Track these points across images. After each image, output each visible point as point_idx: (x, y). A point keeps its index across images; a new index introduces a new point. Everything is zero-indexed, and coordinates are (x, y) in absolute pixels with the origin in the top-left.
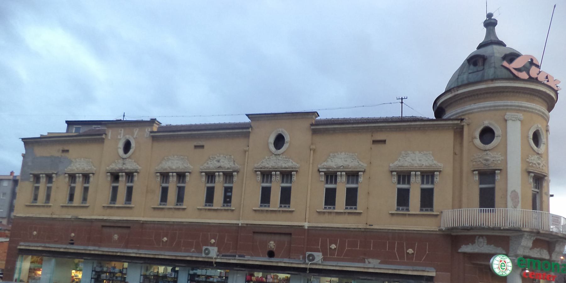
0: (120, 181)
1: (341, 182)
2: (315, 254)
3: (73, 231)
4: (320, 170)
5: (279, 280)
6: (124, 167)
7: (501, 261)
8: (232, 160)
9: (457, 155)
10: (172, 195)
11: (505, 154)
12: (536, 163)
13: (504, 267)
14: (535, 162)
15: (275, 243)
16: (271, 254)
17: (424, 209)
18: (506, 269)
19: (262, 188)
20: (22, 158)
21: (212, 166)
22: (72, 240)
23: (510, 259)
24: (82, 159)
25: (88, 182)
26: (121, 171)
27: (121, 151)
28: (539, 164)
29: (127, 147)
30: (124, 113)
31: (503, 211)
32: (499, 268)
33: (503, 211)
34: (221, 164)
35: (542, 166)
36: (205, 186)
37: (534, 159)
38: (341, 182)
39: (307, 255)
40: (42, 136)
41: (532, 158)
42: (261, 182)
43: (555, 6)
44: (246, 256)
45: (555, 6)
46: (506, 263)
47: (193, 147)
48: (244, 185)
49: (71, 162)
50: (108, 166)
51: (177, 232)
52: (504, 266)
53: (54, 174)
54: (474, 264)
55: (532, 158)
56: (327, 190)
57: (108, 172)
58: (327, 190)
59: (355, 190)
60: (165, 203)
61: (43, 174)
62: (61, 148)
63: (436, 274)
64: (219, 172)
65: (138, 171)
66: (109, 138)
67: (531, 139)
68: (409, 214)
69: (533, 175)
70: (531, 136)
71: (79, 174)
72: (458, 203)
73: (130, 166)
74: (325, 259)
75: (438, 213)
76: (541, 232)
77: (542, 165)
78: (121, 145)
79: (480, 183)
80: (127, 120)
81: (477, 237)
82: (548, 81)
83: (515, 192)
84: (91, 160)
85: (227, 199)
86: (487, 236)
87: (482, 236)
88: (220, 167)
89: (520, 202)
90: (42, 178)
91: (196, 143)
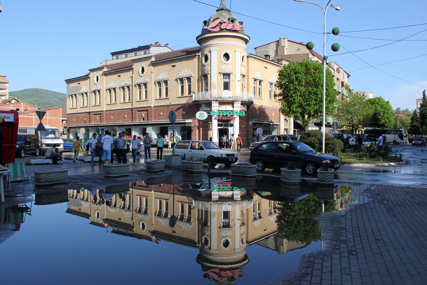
7: (201, 114)
21: (112, 85)
30: (424, 92)
34: (126, 83)
41: (223, 67)
71: (184, 78)
78: (141, 70)
87: (203, 103)
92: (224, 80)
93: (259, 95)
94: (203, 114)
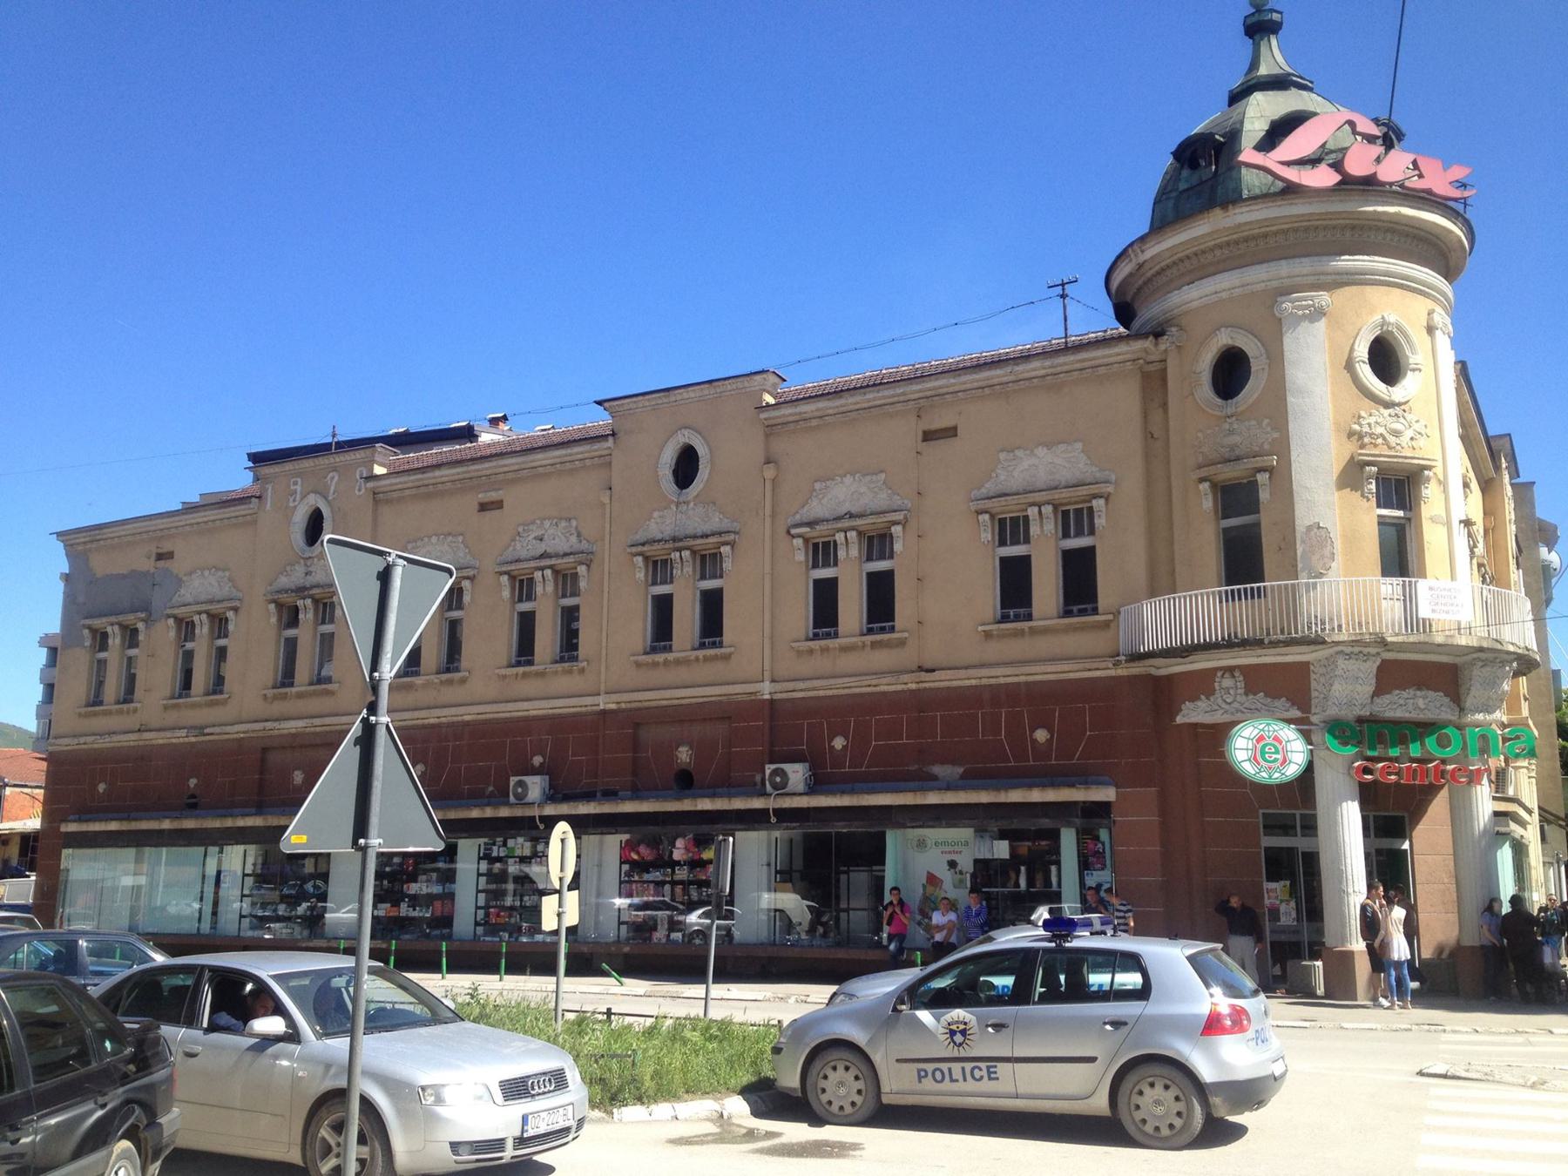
0: (301, 622)
1: (545, 594)
2: (788, 767)
4: (793, 531)
5: (986, 831)
7: (1261, 739)
8: (573, 531)
9: (1154, 441)
12: (1385, 433)
13: (1274, 756)
14: (1379, 430)
15: (691, 748)
17: (1075, 609)
18: (1284, 761)
20: (61, 586)
22: (193, 796)
23: (1410, 824)
25: (575, 593)
26: (301, 591)
27: (298, 536)
28: (1396, 433)
29: (686, 467)
31: (1280, 593)
32: (1255, 758)
33: (1365, 587)
35: (1412, 439)
36: (1057, 546)
37: (1377, 421)
38: (545, 594)
39: (768, 772)
40: (186, 506)
42: (997, 543)
44: (620, 793)
46: (1280, 743)
47: (477, 507)
48: (606, 595)
49: (180, 582)
50: (271, 585)
51: (451, 744)
52: (1277, 752)
55: (1372, 420)
56: (1005, 562)
58: (1005, 562)
59: (1088, 554)
60: (832, 630)
62: (472, 500)
63: (1117, 792)
64: (542, 569)
67: (1364, 362)
68: (1033, 631)
70: (1362, 351)
72: (1162, 581)
74: (816, 784)
75: (1110, 617)
76: (1389, 639)
77: (1409, 433)
78: (669, 456)
79: (1224, 509)
81: (1219, 674)
82: (1421, 176)
83: (1319, 527)
84: (227, 574)
85: (569, 644)
86: (1249, 672)
87: (1230, 670)
88: (544, 556)
89: (1339, 557)
90: (677, 565)
91: (483, 497)
94: (1276, 739)
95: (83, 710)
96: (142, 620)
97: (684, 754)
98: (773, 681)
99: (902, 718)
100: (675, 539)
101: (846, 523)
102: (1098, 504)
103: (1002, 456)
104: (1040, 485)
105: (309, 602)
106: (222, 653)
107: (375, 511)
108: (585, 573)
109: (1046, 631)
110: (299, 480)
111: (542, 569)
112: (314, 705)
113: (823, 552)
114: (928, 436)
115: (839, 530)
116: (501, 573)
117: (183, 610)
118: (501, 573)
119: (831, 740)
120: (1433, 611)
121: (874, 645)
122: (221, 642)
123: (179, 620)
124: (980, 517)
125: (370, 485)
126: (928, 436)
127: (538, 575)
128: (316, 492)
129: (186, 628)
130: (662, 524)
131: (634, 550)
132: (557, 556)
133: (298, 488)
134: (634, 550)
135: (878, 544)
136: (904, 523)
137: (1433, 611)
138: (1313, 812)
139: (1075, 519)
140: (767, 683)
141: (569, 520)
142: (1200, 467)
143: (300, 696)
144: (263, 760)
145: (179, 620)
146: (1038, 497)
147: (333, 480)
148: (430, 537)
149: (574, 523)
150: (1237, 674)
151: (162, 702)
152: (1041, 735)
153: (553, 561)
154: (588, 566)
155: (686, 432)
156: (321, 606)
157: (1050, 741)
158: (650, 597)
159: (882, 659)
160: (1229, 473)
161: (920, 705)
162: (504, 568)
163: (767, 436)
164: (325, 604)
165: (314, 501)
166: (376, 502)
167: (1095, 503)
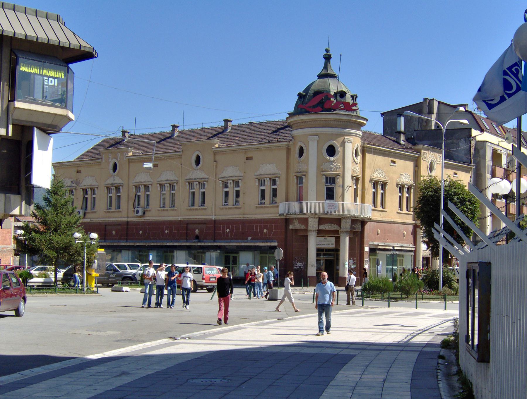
3: (265, 228)
6: (114, 182)
10: (168, 202)
11: (307, 165)
16: (197, 237)
19: (327, 188)
24: (89, 177)
26: (112, 184)
29: (198, 161)
43: (341, 55)
45: (341, 55)
53: (150, 184)
54: (499, 230)
57: (256, 178)
61: (88, 188)
64: (167, 183)
65: (122, 185)
66: (104, 161)
68: (265, 207)
69: (355, 178)
73: (118, 181)
78: (194, 158)
80: (469, 110)
87: (296, 218)
88: (167, 180)
92: (327, 185)
93: (382, 204)
95: (106, 210)
96: (175, 183)
97: (197, 231)
98: (215, 215)
99: (258, 226)
100: (195, 179)
101: (167, 182)
102: (277, 179)
103: (261, 165)
104: (267, 173)
105: (114, 187)
106: (173, 195)
107: (129, 164)
108: (278, 180)
109: (267, 207)
110: (111, 154)
111: (167, 183)
112: (116, 215)
113: (262, 183)
114: (247, 159)
115: (265, 178)
116: (158, 184)
117: (261, 176)
118: (158, 184)
119: (226, 229)
120: (328, 208)
121: (236, 208)
122: (94, 196)
123: (83, 190)
124: (323, 176)
125: (128, 158)
126: (247, 159)
127: (166, 185)
128: (115, 158)
129: (85, 191)
130: (110, 181)
131: (186, 181)
132: (170, 180)
133: (111, 156)
134: (186, 181)
135: (237, 184)
136: (242, 180)
137: (328, 208)
138: (318, 252)
139: (274, 181)
140: (214, 216)
141: (173, 171)
142: (295, 173)
143: (230, 208)
144: (105, 228)
145: (83, 190)
146: (267, 176)
147: (119, 155)
148: (142, 173)
149: (174, 172)
150: (297, 220)
151: (186, 208)
152: (265, 231)
153: (169, 182)
154: (177, 184)
155: (198, 152)
156: (146, 187)
157: (267, 232)
158: (224, 191)
159: (237, 211)
160: (299, 174)
161: (243, 222)
162: (159, 183)
163: (215, 155)
164: (147, 187)
165: (115, 160)
166: (129, 162)
167: (276, 178)
